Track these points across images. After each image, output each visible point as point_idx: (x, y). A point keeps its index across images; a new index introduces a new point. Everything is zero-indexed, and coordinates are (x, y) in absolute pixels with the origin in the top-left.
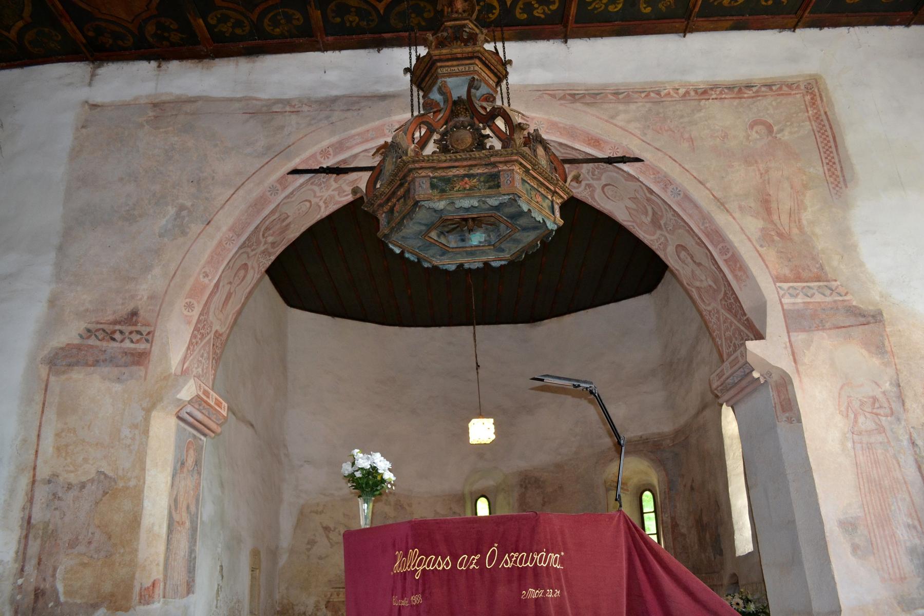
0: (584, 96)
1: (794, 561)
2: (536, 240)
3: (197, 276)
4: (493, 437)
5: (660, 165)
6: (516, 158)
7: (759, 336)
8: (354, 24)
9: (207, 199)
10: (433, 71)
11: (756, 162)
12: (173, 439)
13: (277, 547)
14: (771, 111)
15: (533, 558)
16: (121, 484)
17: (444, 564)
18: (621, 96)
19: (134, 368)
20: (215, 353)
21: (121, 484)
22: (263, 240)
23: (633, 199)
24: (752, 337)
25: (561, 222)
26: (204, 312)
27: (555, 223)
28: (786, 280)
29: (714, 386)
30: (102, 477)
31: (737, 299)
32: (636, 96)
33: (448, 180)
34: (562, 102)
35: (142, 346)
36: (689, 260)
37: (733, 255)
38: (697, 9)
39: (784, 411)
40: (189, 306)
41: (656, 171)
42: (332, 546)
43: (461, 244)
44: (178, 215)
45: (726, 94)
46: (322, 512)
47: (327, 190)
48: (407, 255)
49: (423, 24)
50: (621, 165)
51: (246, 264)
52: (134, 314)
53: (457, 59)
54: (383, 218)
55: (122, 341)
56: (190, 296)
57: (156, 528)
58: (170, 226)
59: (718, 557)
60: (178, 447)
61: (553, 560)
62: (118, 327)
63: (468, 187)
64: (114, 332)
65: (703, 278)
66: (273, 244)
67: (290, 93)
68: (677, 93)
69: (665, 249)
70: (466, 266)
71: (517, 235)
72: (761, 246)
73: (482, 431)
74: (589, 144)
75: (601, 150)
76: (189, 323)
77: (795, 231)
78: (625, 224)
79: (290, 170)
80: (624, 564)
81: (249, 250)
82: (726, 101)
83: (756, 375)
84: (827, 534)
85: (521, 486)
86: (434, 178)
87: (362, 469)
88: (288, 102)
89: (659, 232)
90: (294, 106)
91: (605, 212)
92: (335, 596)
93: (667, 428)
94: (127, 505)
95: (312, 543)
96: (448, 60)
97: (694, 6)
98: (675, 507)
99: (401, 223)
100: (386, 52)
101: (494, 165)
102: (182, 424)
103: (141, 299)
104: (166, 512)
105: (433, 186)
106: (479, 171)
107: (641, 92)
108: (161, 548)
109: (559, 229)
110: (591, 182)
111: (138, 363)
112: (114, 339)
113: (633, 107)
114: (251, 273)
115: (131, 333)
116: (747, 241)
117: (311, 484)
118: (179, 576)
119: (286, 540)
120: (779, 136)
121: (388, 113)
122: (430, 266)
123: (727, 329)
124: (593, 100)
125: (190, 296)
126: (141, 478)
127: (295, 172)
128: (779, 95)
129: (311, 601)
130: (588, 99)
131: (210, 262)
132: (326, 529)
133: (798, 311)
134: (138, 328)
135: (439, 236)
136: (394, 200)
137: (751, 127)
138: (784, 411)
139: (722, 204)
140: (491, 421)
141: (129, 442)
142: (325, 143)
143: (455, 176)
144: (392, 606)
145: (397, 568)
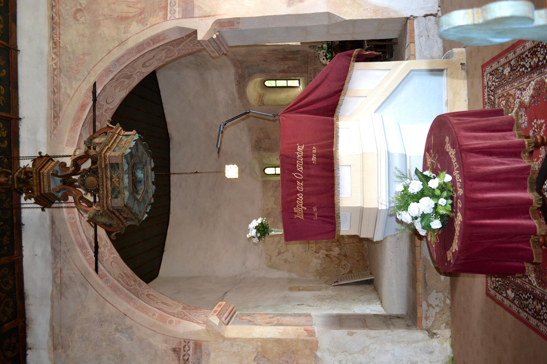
0: (55, 111)
1: (305, 29)
2: (142, 145)
3: (157, 319)
4: (235, 166)
5: (99, 73)
6: (103, 155)
7: (195, 32)
8: (8, 239)
9: (112, 317)
10: (45, 195)
11: (99, 20)
12: (238, 326)
13: (288, 279)
14: (68, 8)
15: (299, 158)
16: (260, 349)
17: (301, 197)
18: (56, 90)
19: (203, 347)
20: (193, 309)
21: (260, 349)
22: (134, 286)
23: (115, 88)
24: (194, 35)
25: (134, 132)
26: (173, 315)
27: (134, 135)
28: (166, 15)
29: (217, 55)
30: (256, 359)
31: (174, 41)
32: (56, 82)
33: (113, 190)
34: (58, 123)
35: (192, 345)
36: (151, 61)
37: (151, 40)
38: (5, 43)
39: (234, 25)
40: (171, 322)
41: (101, 76)
42: (288, 250)
43: (143, 183)
44: (120, 331)
45: (56, 31)
46: (271, 256)
47: (105, 253)
48: (148, 211)
49: (8, 200)
50: (97, 94)
51: (147, 295)
52: (174, 350)
53: (40, 183)
54: (129, 223)
55: (189, 355)
56: (165, 322)
57: (281, 331)
58: (127, 335)
59: (300, 53)
60: (242, 323)
61: (300, 149)
62: (181, 358)
63: (117, 180)
64: (184, 359)
65: (161, 55)
66: (135, 281)
67: (49, 274)
68: (55, 59)
69: (143, 73)
70: (153, 180)
71: (140, 154)
72: (147, 25)
73: (232, 171)
74: (84, 110)
75: (87, 104)
76: (179, 322)
77: (139, 5)
78: (127, 93)
79: (95, 273)
80: (303, 115)
81: (139, 294)
82: (61, 32)
83: (215, 37)
84: (294, 13)
85: (260, 150)
86: (112, 196)
87: (256, 233)
88: (55, 276)
89: (134, 76)
90: (57, 272)
91: (120, 103)
92: (313, 249)
93: (232, 70)
94: (270, 345)
95: (286, 261)
96: (40, 187)
97: (3, 45)
98: (274, 70)
99: (134, 214)
100: (23, 221)
101: (106, 165)
102: (231, 323)
103: (167, 347)
104: (273, 327)
105: (116, 197)
106: (109, 173)
107: (54, 79)
108: (290, 328)
109: (138, 132)
110: (104, 110)
111: (200, 346)
112: (188, 359)
113: (63, 84)
114: (151, 293)
115: (184, 351)
116: (144, 32)
117: (255, 262)
118: (302, 320)
119: (284, 274)
120: (83, 6)
121: (63, 220)
122: (153, 199)
123: (189, 46)
124: (58, 107)
125: (165, 322)
126: (257, 340)
127: (96, 270)
128: (58, 2)
129: (315, 261)
130: (57, 109)
131: (147, 313)
132: (279, 253)
133: (183, 11)
134: (182, 347)
135: (139, 194)
136: (121, 217)
137: (77, 20)
138: (234, 25)
139: (122, 42)
140: (226, 166)
141: (239, 347)
142: (80, 254)
143: (111, 186)
144: (318, 220)
145: (302, 217)
